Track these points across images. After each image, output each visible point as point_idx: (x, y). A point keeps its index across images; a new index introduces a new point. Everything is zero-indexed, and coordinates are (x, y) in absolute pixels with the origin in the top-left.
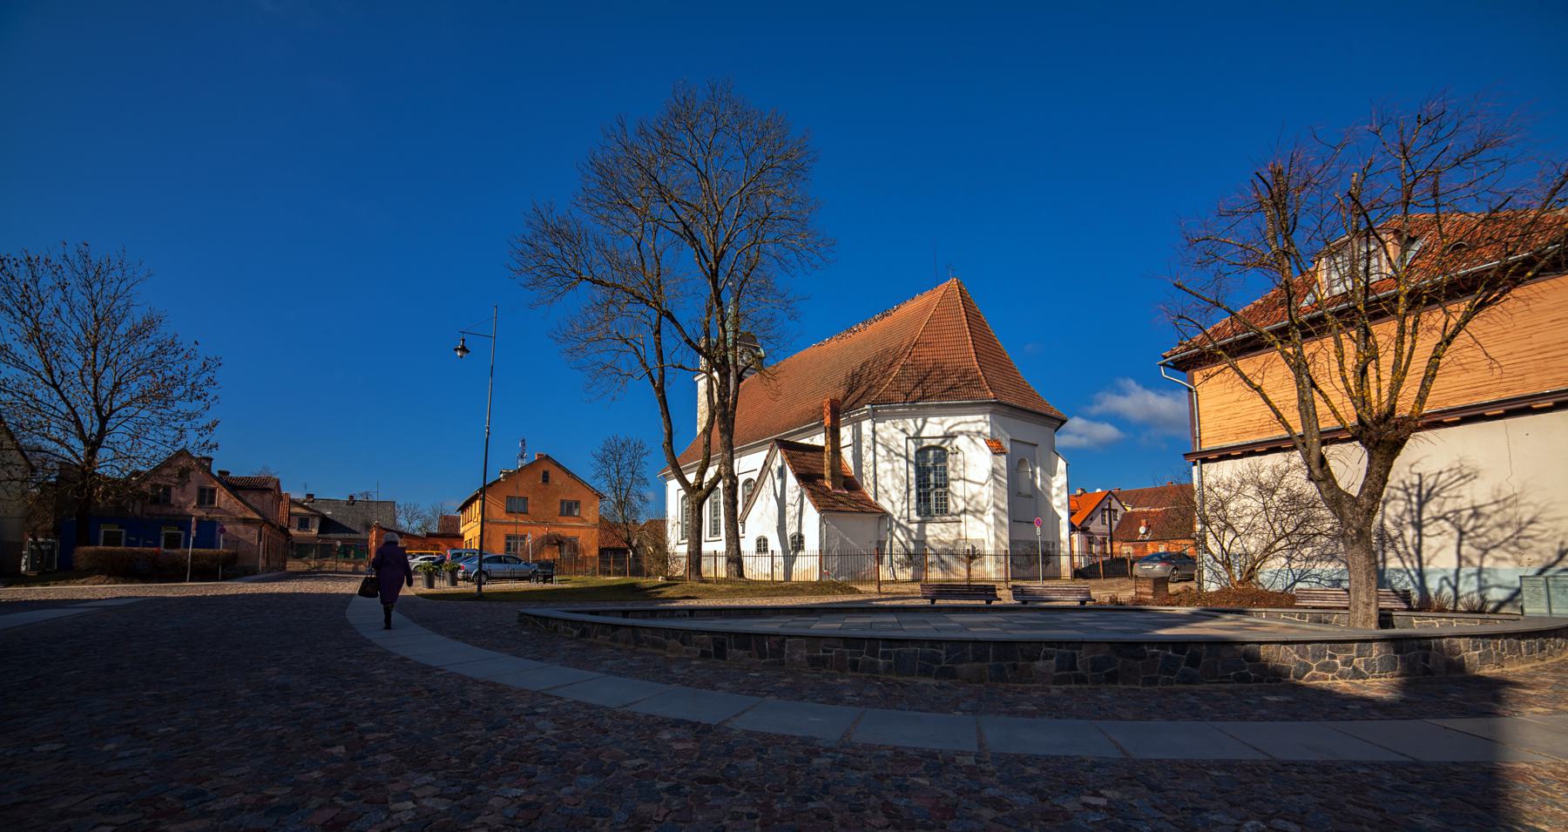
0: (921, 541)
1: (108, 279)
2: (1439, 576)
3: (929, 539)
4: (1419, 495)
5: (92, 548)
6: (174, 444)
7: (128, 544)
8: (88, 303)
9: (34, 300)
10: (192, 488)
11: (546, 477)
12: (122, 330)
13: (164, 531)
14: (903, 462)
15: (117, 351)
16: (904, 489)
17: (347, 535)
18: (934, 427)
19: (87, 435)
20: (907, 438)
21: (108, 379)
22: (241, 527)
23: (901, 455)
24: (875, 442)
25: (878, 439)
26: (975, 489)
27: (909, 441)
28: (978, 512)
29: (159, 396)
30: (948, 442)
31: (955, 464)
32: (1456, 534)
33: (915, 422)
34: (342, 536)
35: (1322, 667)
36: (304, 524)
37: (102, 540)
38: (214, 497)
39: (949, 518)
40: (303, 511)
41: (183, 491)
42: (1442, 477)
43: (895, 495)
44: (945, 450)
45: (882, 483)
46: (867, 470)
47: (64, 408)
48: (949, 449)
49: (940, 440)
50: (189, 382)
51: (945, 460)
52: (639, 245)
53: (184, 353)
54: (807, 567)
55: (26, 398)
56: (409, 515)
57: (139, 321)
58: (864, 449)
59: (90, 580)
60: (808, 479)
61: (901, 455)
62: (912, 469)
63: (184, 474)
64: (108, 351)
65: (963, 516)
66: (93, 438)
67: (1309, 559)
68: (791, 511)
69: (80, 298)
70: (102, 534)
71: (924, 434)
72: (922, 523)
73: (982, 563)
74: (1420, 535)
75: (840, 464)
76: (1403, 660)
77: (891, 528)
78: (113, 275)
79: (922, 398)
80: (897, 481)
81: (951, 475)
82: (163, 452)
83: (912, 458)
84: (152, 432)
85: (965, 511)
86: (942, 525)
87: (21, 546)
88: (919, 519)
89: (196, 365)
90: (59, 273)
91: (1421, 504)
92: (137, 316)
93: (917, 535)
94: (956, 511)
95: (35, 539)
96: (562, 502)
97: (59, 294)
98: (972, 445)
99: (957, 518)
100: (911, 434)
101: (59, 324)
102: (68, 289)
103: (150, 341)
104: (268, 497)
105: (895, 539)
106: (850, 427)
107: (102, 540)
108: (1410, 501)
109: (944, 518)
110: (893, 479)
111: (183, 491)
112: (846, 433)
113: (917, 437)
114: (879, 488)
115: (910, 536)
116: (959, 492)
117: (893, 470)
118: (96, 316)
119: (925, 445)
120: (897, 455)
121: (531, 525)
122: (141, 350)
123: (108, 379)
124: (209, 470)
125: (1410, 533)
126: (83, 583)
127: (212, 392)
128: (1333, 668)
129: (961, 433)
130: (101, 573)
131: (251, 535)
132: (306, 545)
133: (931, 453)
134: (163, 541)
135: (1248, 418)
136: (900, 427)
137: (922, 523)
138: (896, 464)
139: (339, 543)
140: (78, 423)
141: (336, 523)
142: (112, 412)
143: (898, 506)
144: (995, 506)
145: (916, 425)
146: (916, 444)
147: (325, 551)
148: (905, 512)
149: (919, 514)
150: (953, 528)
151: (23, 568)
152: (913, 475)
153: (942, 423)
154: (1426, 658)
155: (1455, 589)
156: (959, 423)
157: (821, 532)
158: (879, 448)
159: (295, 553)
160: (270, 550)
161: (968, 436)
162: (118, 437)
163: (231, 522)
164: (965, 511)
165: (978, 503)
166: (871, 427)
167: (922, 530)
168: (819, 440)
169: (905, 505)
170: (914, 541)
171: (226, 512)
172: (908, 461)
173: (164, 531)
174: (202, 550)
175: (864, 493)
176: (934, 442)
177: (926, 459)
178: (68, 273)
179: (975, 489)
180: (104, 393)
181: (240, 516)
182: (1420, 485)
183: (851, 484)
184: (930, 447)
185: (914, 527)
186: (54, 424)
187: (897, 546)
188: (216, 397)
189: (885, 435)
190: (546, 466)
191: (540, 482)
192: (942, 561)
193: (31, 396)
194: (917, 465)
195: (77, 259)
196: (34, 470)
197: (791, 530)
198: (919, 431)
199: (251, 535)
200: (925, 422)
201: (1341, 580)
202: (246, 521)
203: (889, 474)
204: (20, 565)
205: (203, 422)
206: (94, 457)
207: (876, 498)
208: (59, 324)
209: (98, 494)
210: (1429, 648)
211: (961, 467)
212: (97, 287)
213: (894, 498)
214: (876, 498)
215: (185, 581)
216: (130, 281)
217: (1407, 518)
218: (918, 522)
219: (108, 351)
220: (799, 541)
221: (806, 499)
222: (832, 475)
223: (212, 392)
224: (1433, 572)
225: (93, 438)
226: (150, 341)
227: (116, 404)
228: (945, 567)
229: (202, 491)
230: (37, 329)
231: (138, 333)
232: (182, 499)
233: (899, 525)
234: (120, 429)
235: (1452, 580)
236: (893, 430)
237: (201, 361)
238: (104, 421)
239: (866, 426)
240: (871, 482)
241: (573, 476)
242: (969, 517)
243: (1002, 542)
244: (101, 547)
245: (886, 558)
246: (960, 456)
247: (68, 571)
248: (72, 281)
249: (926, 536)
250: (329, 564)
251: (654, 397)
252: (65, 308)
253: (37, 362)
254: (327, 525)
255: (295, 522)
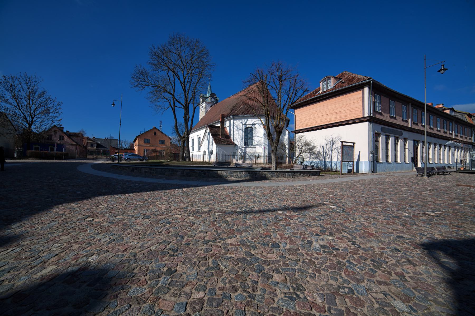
0: (245, 153)
1: (32, 82)
2: (334, 163)
3: (247, 152)
4: (332, 143)
5: (31, 151)
6: (51, 124)
7: (41, 150)
8: (27, 88)
9: (13, 87)
10: (58, 135)
11: (155, 133)
12: (37, 94)
13: (50, 147)
14: (241, 131)
15: (35, 100)
16: (241, 138)
17: (104, 149)
18: (250, 122)
19: (28, 121)
20: (242, 125)
21: (33, 108)
22: (71, 146)
23: (241, 129)
24: (234, 126)
25: (235, 125)
26: (260, 139)
27: (243, 126)
28: (260, 145)
29: (47, 112)
30: (253, 126)
31: (255, 132)
32: (337, 153)
33: (245, 120)
34: (103, 149)
35: (231, 176)
36: (92, 145)
37: (34, 149)
38: (63, 138)
39: (253, 147)
40: (92, 142)
41: (55, 136)
42: (336, 139)
43: (239, 140)
44: (253, 128)
45: (235, 137)
46: (232, 133)
47: (22, 115)
48: (254, 128)
49: (251, 125)
50: (54, 108)
51: (253, 131)
52: (168, 74)
53: (53, 100)
54: (213, 159)
55: (13, 113)
56: (125, 143)
57: (41, 92)
58: (231, 127)
59: (31, 159)
60: (215, 136)
61: (241, 129)
62: (243, 133)
63: (55, 132)
64: (33, 101)
65: (256, 146)
66: (30, 123)
67: (313, 158)
68: (211, 144)
69: (25, 86)
70: (34, 147)
71: (247, 124)
72: (246, 148)
73: (261, 159)
74: (332, 153)
75: (224, 132)
76: (250, 175)
77: (237, 149)
78: (33, 81)
79: (247, 114)
80: (239, 136)
81: (254, 135)
82: (48, 127)
83: (244, 130)
84: (45, 121)
85: (257, 145)
86: (251, 148)
87: (14, 150)
88: (245, 146)
89: (56, 104)
90: (19, 80)
91: (332, 145)
92: (40, 91)
93: (244, 151)
94: (255, 145)
95: (18, 148)
96: (160, 140)
97: (20, 86)
98: (259, 127)
99: (255, 147)
100: (244, 124)
101: (20, 93)
102: (22, 84)
103: (44, 97)
104: (79, 138)
105: (238, 152)
106: (229, 121)
107: (34, 149)
108: (331, 144)
109: (251, 146)
110: (238, 136)
111: (55, 136)
112: (227, 124)
113: (245, 124)
114: (234, 138)
115: (242, 151)
116: (256, 140)
117: (238, 133)
118: (29, 91)
119: (247, 127)
120: (240, 129)
121: (151, 147)
122: (42, 100)
123: (33, 108)
124: (62, 131)
125: (330, 152)
126: (29, 160)
127: (60, 111)
128: (233, 176)
129: (257, 124)
130: (33, 157)
131: (73, 148)
132: (93, 151)
133: (249, 129)
134: (49, 150)
135: (304, 122)
136: (241, 122)
137: (246, 148)
138: (239, 132)
139: (102, 151)
140: (26, 119)
141: (101, 145)
142: (35, 116)
143: (239, 143)
144: (264, 143)
145: (245, 121)
146: (245, 126)
147: (98, 153)
148: (241, 145)
149: (245, 145)
150: (254, 149)
151: (15, 156)
152: (244, 135)
153: (252, 121)
154: (256, 175)
155: (336, 166)
156: (256, 121)
157: (216, 150)
158: (235, 127)
159: (90, 154)
160: (80, 153)
161: (259, 124)
162: (37, 123)
163: (68, 145)
164: (257, 145)
165: (260, 143)
166: (233, 122)
167: (245, 149)
168: (219, 125)
169: (241, 143)
170: (243, 152)
171: (67, 142)
172: (242, 131)
173: (50, 147)
174: (58, 152)
175: (231, 139)
176: (250, 126)
177: (248, 130)
178: (22, 80)
179: (260, 139)
180: (32, 111)
181: (71, 143)
182: (332, 141)
183: (228, 137)
184: (249, 127)
185: (243, 149)
186: (20, 119)
187: (239, 154)
188: (61, 112)
189: (237, 124)
190: (155, 130)
191: (154, 135)
192: (250, 158)
193: (14, 112)
194: (245, 132)
195: (24, 77)
196: (16, 130)
197: (210, 149)
198: (246, 123)
199: (73, 148)
200: (247, 120)
201: (318, 164)
202: (72, 145)
203: (237, 134)
204: (14, 155)
205: (58, 119)
206: (30, 128)
207: (234, 141)
208: (20, 93)
209: (32, 137)
210: (257, 173)
211: (256, 133)
212: (29, 84)
213: (238, 141)
214: (234, 141)
215: (54, 159)
216: (38, 82)
217: (330, 149)
218: (244, 147)
219: (33, 101)
220: (212, 151)
221: (213, 141)
222: (221, 134)
223: (60, 111)
224: (333, 162)
225: (30, 123)
226: (44, 97)
227: (35, 114)
228: (251, 159)
229: (60, 136)
230: (15, 95)
231: (40, 96)
232: (55, 139)
233: (239, 148)
234: (37, 120)
235: (336, 164)
236: (239, 123)
237: (57, 103)
238: (33, 118)
239: (232, 121)
240: (233, 136)
241: (163, 133)
242: (258, 146)
243: (266, 153)
244: (34, 151)
245: (236, 157)
246: (256, 130)
247: (25, 157)
248: (23, 83)
249: (246, 151)
250: (99, 157)
251: (173, 113)
252: (21, 89)
253: (15, 103)
254: (99, 146)
255: (89, 145)
